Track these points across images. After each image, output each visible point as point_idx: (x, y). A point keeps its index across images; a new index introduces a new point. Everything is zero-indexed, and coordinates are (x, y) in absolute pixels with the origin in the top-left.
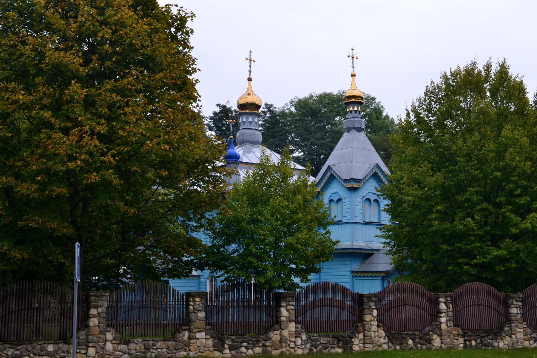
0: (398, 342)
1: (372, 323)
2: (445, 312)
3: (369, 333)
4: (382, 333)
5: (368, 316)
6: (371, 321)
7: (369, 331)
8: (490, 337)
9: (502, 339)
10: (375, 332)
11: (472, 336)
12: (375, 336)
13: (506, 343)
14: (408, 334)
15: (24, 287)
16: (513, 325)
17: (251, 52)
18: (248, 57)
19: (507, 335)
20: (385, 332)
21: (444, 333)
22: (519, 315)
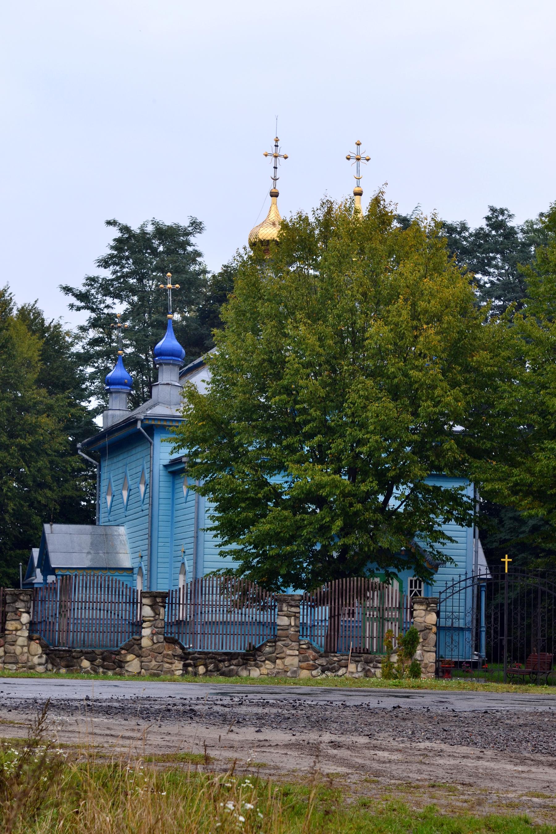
0: (63, 663)
1: (19, 633)
2: (149, 621)
3: (12, 648)
4: (36, 648)
5: (13, 622)
6: (17, 630)
7: (13, 645)
8: (234, 662)
9: (258, 667)
10: (22, 646)
11: (199, 658)
12: (22, 653)
13: (265, 672)
14: (81, 651)
15: (332, 645)
16: (279, 643)
17: (277, 141)
18: (271, 149)
19: (267, 659)
20: (42, 647)
21: (145, 652)
22: (292, 629)
